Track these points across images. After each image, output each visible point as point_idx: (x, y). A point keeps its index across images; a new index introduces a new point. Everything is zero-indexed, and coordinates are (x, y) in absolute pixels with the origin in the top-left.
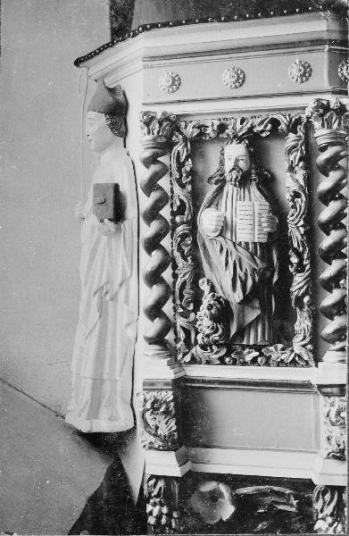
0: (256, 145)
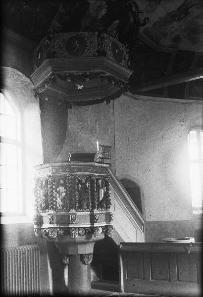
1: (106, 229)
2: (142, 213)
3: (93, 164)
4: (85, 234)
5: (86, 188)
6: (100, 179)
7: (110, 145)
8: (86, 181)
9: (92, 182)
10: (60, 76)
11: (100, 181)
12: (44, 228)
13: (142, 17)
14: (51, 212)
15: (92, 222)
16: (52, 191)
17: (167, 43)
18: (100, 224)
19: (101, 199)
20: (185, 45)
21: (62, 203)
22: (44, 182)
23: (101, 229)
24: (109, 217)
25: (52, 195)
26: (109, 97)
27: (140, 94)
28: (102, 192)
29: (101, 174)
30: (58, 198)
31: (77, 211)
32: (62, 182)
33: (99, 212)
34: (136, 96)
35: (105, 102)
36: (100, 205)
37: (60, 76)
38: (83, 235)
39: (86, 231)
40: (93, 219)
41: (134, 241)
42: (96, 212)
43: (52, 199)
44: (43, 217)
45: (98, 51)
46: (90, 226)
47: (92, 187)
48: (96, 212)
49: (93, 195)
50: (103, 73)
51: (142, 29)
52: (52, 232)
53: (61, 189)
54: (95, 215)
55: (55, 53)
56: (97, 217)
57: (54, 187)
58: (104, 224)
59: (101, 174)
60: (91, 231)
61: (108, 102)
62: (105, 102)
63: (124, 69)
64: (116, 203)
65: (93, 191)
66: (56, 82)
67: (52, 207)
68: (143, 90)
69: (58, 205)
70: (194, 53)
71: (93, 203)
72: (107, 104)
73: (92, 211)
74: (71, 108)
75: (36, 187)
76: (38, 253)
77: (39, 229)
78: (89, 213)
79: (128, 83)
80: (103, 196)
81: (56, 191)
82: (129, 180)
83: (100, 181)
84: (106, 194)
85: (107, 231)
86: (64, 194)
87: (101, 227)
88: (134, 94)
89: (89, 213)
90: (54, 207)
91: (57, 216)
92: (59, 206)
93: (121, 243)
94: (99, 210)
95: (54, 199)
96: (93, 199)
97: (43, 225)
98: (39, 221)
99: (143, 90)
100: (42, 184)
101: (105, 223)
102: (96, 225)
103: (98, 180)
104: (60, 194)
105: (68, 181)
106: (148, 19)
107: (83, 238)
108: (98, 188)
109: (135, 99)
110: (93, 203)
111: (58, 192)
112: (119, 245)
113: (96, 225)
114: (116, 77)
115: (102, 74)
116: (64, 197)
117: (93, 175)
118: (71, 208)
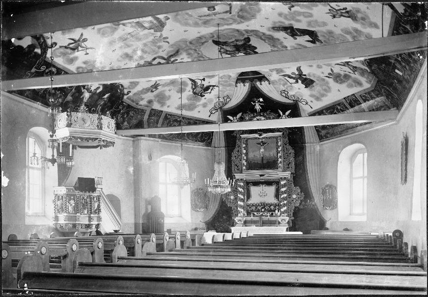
0: (62, 197)
1: (98, 226)
2: (121, 218)
5: (87, 203)
8: (87, 197)
13: (126, 91)
14: (66, 214)
15: (90, 221)
17: (143, 103)
18: (94, 222)
20: (156, 106)
24: (99, 219)
28: (96, 205)
40: (90, 219)
43: (66, 207)
48: (92, 215)
51: (125, 97)
58: (97, 223)
60: (88, 226)
70: (162, 111)
74: (76, 149)
81: (69, 202)
84: (99, 206)
86: (74, 205)
98: (57, 218)
103: (94, 197)
106: (130, 92)
107: (153, 237)
112: (285, 212)
113: (92, 223)
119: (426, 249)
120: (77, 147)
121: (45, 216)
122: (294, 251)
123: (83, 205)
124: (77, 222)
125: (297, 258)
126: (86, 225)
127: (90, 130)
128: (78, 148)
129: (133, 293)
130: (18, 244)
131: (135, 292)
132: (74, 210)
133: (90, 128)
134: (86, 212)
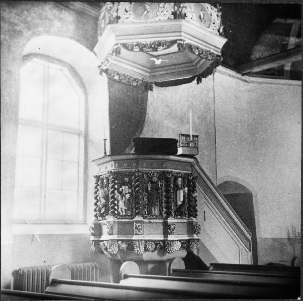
0: (108, 180)
3: (172, 157)
4: (156, 249)
6: (179, 177)
7: (197, 135)
9: (168, 180)
10: (125, 46)
11: (180, 179)
12: (103, 241)
15: (166, 234)
16: (113, 192)
19: (179, 203)
21: (125, 208)
22: (105, 181)
23: (179, 244)
24: (192, 229)
25: (113, 197)
26: (200, 75)
27: (250, 74)
29: (182, 171)
30: (120, 201)
31: (145, 218)
32: (126, 179)
33: (176, 221)
34: (246, 78)
35: (195, 81)
36: (179, 213)
37: (125, 46)
38: (153, 251)
39: (156, 244)
41: (237, 263)
42: (171, 220)
43: (112, 202)
44: (103, 226)
45: (174, 14)
46: (162, 238)
47: (167, 186)
48: (171, 220)
49: (168, 197)
50: (181, 40)
52: (110, 246)
53: (125, 189)
54: (170, 225)
55: (118, 18)
56: (173, 227)
57: (116, 186)
58: (185, 237)
59: (182, 171)
61: (199, 81)
62: (195, 81)
63: (213, 36)
64: (206, 209)
65: (167, 191)
66: (120, 53)
67: (113, 212)
68: (256, 70)
69: (119, 210)
71: (168, 208)
72: (198, 83)
73: (166, 219)
74: (151, 90)
75: (96, 188)
76: (96, 273)
77: (97, 243)
78: (161, 221)
79: (220, 54)
80: (182, 199)
81: (118, 192)
82: (236, 183)
83: (180, 179)
85: (188, 247)
86: (128, 196)
87: (180, 241)
88: (243, 75)
89: (161, 221)
90: (116, 212)
91: (119, 223)
92: (122, 211)
93: (211, 264)
94: (178, 218)
95: (116, 202)
96: (168, 202)
97: (102, 237)
99: (256, 70)
100: (102, 182)
101: (117, 236)
102: (170, 238)
103: (176, 178)
104: (123, 196)
105: (135, 178)
108: (177, 188)
109: (245, 81)
110: (168, 208)
111: (121, 193)
112: (209, 267)
113: (170, 238)
114: (200, 46)
115: (180, 42)
116: (129, 200)
117: (168, 171)
118: (137, 214)
119: (299, 230)
120: (154, 86)
121: (85, 223)
122: (44, 166)
123: (150, 195)
124: (135, 237)
125: (224, 212)
126: (156, 242)
127: (159, 24)
128: (155, 88)
129: (275, 84)
130: (23, 285)
131: (273, 86)
132: (130, 209)
133: (157, 19)
134: (156, 211)
